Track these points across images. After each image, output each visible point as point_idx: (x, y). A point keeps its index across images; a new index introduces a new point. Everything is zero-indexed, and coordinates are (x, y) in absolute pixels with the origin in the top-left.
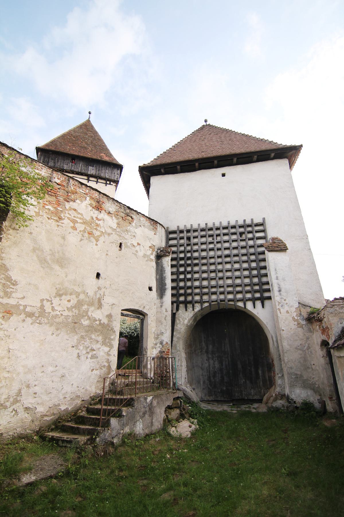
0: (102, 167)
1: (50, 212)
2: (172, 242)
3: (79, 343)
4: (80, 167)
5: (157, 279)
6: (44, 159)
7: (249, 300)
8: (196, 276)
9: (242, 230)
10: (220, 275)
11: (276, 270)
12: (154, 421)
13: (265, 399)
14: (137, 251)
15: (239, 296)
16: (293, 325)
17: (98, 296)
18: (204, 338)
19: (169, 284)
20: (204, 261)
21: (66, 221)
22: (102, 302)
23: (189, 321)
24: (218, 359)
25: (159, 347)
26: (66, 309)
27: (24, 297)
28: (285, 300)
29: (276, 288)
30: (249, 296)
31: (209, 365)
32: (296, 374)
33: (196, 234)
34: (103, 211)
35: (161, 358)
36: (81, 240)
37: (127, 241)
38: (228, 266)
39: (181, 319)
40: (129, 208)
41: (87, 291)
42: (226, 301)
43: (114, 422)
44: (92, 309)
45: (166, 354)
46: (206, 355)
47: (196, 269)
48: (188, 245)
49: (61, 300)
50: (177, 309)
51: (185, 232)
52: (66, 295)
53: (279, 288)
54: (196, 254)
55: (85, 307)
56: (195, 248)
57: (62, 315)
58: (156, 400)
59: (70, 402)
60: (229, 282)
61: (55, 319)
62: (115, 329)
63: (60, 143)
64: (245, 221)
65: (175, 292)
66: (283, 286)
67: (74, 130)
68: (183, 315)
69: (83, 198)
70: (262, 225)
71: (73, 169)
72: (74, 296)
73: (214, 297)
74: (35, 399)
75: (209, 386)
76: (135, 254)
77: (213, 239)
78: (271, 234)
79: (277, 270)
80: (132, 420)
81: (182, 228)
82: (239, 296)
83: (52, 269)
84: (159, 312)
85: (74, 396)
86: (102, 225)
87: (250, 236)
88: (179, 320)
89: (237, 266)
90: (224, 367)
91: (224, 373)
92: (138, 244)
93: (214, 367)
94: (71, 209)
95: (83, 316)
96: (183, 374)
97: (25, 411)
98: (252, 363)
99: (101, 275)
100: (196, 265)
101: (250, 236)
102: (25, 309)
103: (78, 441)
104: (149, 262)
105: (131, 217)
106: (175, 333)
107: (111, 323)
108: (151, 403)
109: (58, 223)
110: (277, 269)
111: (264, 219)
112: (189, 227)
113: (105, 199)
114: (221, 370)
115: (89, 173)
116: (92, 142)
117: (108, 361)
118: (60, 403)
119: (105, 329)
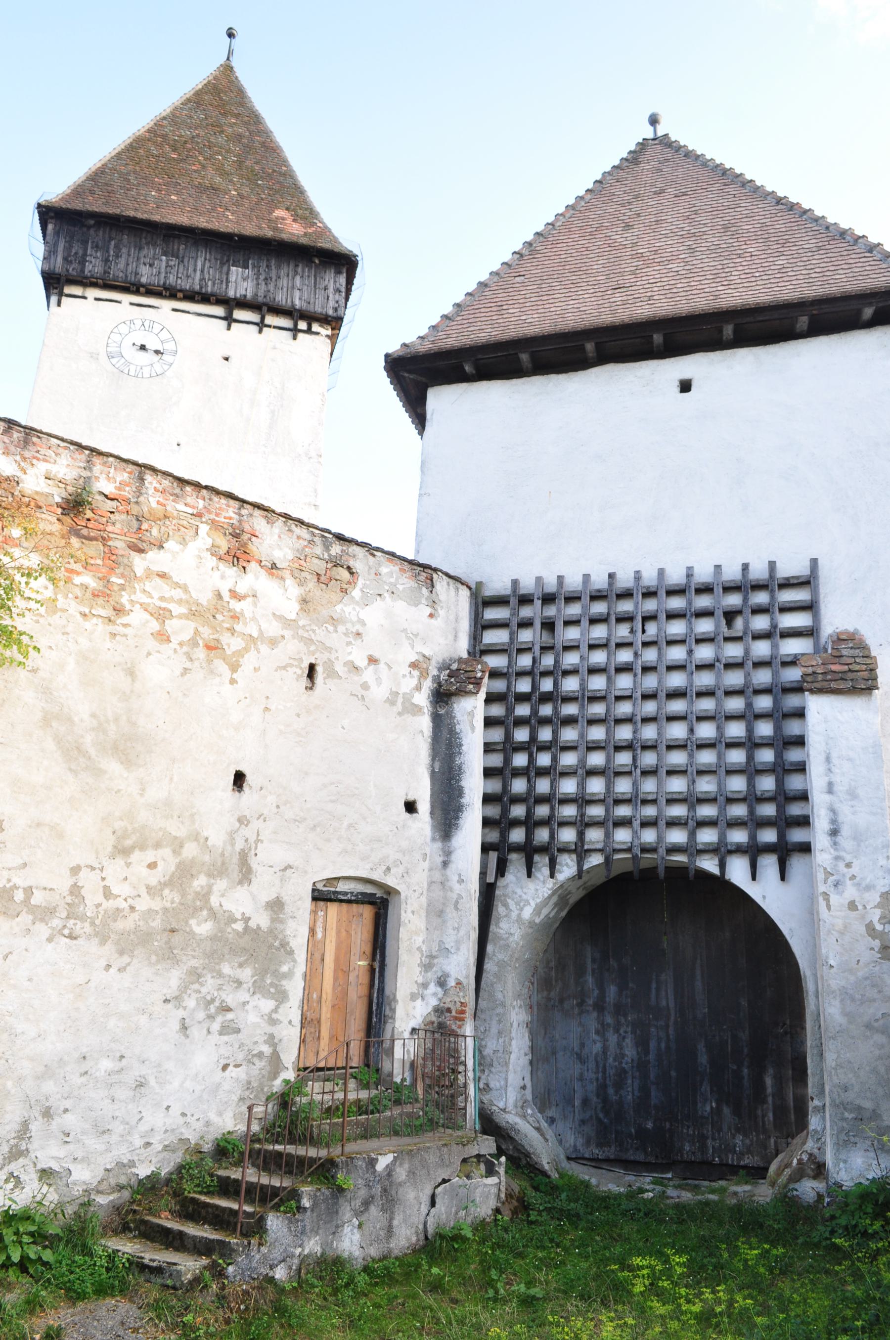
0: (278, 267)
1: (88, 595)
2: (492, 637)
3: (184, 989)
4: (199, 269)
5: (433, 774)
6: (68, 249)
7: (739, 850)
8: (569, 759)
9: (734, 600)
10: (649, 759)
11: (828, 759)
12: (395, 1223)
13: (773, 1168)
14: (365, 686)
15: (707, 836)
16: (866, 950)
17: (239, 845)
18: (594, 961)
19: (474, 786)
20: (598, 709)
21: (137, 617)
22: (253, 862)
23: (537, 911)
24: (633, 1032)
25: (435, 994)
26: (143, 891)
27: (25, 865)
28: (848, 865)
29: (821, 823)
30: (739, 836)
31: (605, 1050)
32: (859, 1108)
33: (574, 610)
34: (253, 566)
35: (441, 1031)
36: (186, 670)
37: (333, 657)
38: (678, 731)
39: (511, 904)
40: (340, 538)
41: (205, 834)
42: (662, 851)
43: (274, 1222)
44: (220, 885)
45: (456, 1018)
46: (595, 1014)
47: (569, 734)
48: (544, 649)
49: (128, 865)
50: (501, 870)
51: (538, 603)
52: (143, 848)
53: (834, 821)
54: (571, 684)
55: (201, 881)
56: (571, 659)
57: (132, 908)
58: (406, 1166)
59: (161, 1156)
60: (677, 785)
61: (115, 920)
62: (293, 944)
63: (125, 177)
64: (745, 567)
65: (494, 811)
66: (846, 816)
67: (173, 118)
68: (519, 891)
69: (186, 532)
70: (806, 582)
71: (172, 280)
72: (166, 852)
73: (622, 836)
74: (67, 1147)
75: (601, 1115)
76: (361, 696)
77: (632, 631)
78: (835, 619)
79: (835, 761)
80: (329, 1217)
81: (527, 585)
82: (707, 836)
83: (99, 773)
84: (441, 885)
85: (171, 1139)
86: (248, 614)
87: (761, 623)
88: (506, 905)
89: (706, 731)
90: (652, 1057)
91: (652, 1076)
92: (372, 660)
93: (620, 1056)
94: (149, 574)
95: (196, 910)
96: (511, 1076)
97: (40, 1179)
98: (746, 1050)
99: (249, 778)
100: (570, 721)
101: (761, 623)
102: (29, 899)
103: (179, 1272)
104: (408, 718)
105: (349, 568)
106: (490, 948)
107: (280, 926)
108: (389, 1175)
109: (111, 628)
110: (834, 755)
111: (814, 562)
112: (551, 585)
113: (258, 522)
114: (641, 1066)
115: (231, 294)
116: (240, 164)
117: (271, 1040)
118: (136, 1158)
119: (260, 949)
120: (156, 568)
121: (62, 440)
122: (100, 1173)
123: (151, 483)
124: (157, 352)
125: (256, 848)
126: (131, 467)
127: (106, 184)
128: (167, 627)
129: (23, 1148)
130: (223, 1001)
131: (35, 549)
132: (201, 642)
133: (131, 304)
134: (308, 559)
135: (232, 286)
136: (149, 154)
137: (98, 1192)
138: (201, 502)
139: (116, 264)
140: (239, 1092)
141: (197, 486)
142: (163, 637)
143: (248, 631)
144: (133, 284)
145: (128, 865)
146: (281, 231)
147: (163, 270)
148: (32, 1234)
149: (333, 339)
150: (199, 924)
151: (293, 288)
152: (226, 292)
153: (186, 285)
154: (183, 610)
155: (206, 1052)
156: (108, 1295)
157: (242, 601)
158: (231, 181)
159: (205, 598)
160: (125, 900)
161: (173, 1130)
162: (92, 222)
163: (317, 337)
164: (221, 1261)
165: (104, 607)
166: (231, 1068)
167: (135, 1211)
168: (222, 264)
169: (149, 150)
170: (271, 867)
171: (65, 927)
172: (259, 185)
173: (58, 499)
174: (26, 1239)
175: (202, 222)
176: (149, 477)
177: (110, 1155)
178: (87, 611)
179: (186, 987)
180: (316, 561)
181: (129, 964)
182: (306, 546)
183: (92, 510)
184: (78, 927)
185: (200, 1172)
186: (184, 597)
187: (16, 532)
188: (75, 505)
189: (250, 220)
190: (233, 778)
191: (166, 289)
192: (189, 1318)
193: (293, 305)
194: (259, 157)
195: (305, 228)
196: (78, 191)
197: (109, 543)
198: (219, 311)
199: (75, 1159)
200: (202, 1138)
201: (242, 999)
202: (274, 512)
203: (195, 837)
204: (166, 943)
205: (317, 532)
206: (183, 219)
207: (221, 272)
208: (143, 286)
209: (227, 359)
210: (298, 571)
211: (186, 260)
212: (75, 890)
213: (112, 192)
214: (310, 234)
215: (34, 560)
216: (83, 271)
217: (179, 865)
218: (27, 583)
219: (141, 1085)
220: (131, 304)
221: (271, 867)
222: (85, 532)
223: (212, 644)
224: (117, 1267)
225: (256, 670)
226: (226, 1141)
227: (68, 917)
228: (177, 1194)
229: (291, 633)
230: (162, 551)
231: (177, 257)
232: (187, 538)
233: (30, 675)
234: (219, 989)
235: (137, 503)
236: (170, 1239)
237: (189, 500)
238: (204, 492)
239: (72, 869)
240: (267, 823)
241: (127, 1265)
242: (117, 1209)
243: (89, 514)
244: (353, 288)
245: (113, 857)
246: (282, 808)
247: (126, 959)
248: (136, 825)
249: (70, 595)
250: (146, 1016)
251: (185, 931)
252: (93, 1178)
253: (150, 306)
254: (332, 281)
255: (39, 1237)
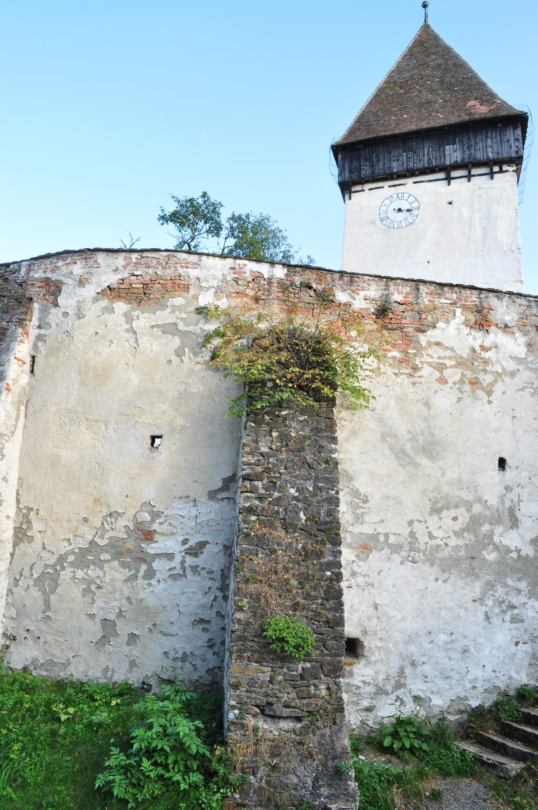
0: (475, 137)
1: (397, 362)
3: (484, 594)
4: (426, 154)
6: (350, 166)
17: (508, 504)
21: (426, 371)
22: (518, 515)
27: (382, 521)
36: (459, 399)
41: (485, 498)
44: (499, 529)
49: (441, 519)
52: (448, 509)
55: (486, 528)
57: (446, 545)
61: (437, 552)
67: (398, 69)
71: (411, 165)
83: (416, 465)
94: (430, 344)
95: (486, 546)
97: (414, 702)
99: (508, 461)
103: (507, 769)
109: (412, 380)
113: (493, 301)
115: (448, 163)
116: (442, 82)
118: (468, 695)
120: (433, 340)
121: (371, 276)
122: (448, 702)
123: (423, 290)
124: (408, 210)
125: (519, 506)
126: (410, 283)
127: (366, 122)
128: (445, 374)
129: (403, 683)
130: (510, 602)
131: (365, 341)
132: (466, 380)
133: (390, 186)
134: (528, 318)
135: (447, 158)
136: (387, 96)
137: (448, 713)
138: (455, 295)
139: (378, 166)
140: (528, 660)
141: (451, 286)
142: (443, 381)
143: (495, 369)
144: (389, 175)
145: (441, 519)
146: (474, 114)
147: (405, 161)
148: (414, 733)
149: (518, 172)
150: (488, 554)
151: (486, 147)
152: (445, 163)
153: (420, 166)
154: (453, 363)
155: (503, 634)
156: (464, 776)
157: (489, 352)
158: (438, 94)
159: (465, 353)
160: (442, 540)
161: (489, 680)
162: (361, 146)
163: (507, 173)
164: (533, 766)
165: (406, 368)
166: (520, 644)
167: (472, 727)
168: (440, 146)
169: (387, 94)
170: (530, 517)
171: (409, 556)
172: (455, 91)
173: (373, 310)
174: (411, 735)
175: (424, 125)
176: (422, 287)
177: (452, 691)
178: (397, 372)
179: (486, 593)
180: (534, 318)
181: (449, 578)
182: (526, 310)
183: (392, 313)
184: (417, 556)
185: (509, 708)
186: (452, 355)
187: (354, 334)
188: (382, 312)
189: (453, 113)
190: (497, 462)
191: (408, 172)
192: (518, 799)
193: (488, 158)
194: (453, 73)
195: (489, 107)
196: (352, 131)
197: (405, 330)
198: (442, 175)
199: (432, 692)
200: (508, 686)
201: (523, 601)
202: (501, 292)
203: (479, 500)
204: (469, 565)
205: (532, 299)
206: (413, 127)
207: (440, 152)
208: (395, 174)
209: (450, 203)
210: (522, 327)
211: (418, 150)
212: (412, 534)
213: (370, 125)
214: (493, 110)
215: (365, 348)
216: (360, 176)
217: (471, 518)
218: (363, 361)
219: (466, 651)
220: (390, 186)
221: (530, 517)
222: (390, 326)
223: (474, 381)
224: (467, 760)
225: (504, 393)
226: (524, 690)
227: (410, 550)
228: (497, 720)
229: (524, 366)
230: (435, 329)
231: (412, 151)
232: (449, 319)
233: (371, 412)
234: (506, 595)
235: (417, 303)
236: (497, 747)
237: (447, 295)
238: (456, 288)
239: (409, 522)
240: (524, 489)
241: (473, 759)
242: (461, 724)
243: (391, 316)
244: (527, 135)
245: (431, 514)
246: (533, 479)
247: (446, 575)
248: (442, 495)
249: (387, 364)
250: (463, 610)
251: (480, 558)
252: (444, 704)
253: (400, 185)
254: (512, 135)
255: (419, 735)
